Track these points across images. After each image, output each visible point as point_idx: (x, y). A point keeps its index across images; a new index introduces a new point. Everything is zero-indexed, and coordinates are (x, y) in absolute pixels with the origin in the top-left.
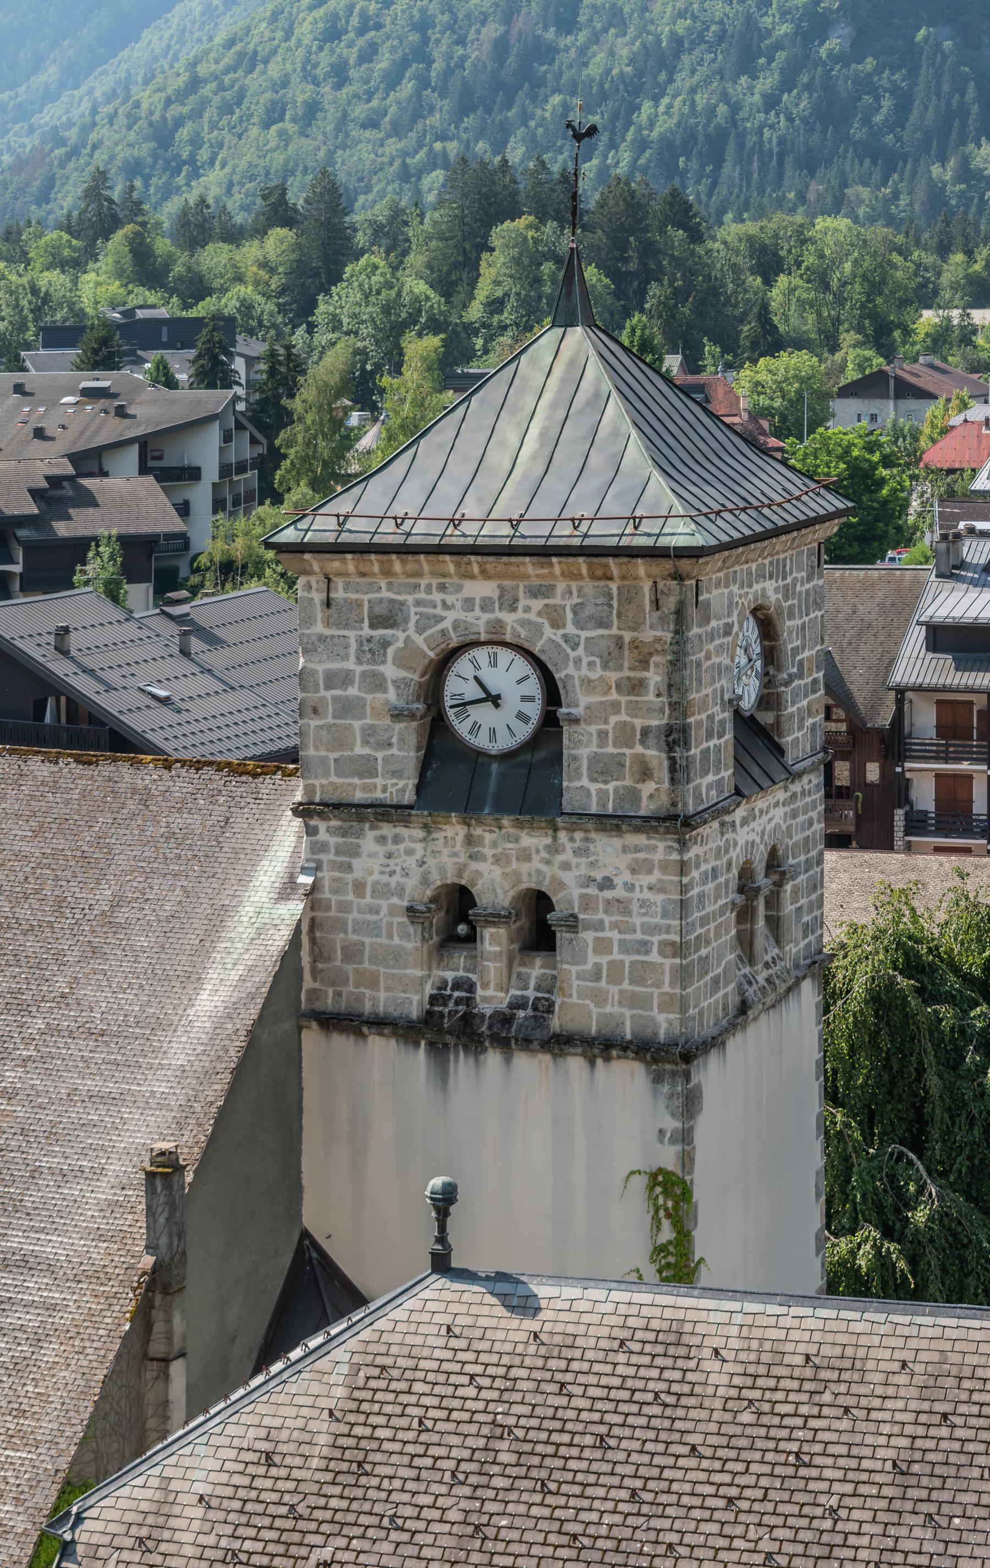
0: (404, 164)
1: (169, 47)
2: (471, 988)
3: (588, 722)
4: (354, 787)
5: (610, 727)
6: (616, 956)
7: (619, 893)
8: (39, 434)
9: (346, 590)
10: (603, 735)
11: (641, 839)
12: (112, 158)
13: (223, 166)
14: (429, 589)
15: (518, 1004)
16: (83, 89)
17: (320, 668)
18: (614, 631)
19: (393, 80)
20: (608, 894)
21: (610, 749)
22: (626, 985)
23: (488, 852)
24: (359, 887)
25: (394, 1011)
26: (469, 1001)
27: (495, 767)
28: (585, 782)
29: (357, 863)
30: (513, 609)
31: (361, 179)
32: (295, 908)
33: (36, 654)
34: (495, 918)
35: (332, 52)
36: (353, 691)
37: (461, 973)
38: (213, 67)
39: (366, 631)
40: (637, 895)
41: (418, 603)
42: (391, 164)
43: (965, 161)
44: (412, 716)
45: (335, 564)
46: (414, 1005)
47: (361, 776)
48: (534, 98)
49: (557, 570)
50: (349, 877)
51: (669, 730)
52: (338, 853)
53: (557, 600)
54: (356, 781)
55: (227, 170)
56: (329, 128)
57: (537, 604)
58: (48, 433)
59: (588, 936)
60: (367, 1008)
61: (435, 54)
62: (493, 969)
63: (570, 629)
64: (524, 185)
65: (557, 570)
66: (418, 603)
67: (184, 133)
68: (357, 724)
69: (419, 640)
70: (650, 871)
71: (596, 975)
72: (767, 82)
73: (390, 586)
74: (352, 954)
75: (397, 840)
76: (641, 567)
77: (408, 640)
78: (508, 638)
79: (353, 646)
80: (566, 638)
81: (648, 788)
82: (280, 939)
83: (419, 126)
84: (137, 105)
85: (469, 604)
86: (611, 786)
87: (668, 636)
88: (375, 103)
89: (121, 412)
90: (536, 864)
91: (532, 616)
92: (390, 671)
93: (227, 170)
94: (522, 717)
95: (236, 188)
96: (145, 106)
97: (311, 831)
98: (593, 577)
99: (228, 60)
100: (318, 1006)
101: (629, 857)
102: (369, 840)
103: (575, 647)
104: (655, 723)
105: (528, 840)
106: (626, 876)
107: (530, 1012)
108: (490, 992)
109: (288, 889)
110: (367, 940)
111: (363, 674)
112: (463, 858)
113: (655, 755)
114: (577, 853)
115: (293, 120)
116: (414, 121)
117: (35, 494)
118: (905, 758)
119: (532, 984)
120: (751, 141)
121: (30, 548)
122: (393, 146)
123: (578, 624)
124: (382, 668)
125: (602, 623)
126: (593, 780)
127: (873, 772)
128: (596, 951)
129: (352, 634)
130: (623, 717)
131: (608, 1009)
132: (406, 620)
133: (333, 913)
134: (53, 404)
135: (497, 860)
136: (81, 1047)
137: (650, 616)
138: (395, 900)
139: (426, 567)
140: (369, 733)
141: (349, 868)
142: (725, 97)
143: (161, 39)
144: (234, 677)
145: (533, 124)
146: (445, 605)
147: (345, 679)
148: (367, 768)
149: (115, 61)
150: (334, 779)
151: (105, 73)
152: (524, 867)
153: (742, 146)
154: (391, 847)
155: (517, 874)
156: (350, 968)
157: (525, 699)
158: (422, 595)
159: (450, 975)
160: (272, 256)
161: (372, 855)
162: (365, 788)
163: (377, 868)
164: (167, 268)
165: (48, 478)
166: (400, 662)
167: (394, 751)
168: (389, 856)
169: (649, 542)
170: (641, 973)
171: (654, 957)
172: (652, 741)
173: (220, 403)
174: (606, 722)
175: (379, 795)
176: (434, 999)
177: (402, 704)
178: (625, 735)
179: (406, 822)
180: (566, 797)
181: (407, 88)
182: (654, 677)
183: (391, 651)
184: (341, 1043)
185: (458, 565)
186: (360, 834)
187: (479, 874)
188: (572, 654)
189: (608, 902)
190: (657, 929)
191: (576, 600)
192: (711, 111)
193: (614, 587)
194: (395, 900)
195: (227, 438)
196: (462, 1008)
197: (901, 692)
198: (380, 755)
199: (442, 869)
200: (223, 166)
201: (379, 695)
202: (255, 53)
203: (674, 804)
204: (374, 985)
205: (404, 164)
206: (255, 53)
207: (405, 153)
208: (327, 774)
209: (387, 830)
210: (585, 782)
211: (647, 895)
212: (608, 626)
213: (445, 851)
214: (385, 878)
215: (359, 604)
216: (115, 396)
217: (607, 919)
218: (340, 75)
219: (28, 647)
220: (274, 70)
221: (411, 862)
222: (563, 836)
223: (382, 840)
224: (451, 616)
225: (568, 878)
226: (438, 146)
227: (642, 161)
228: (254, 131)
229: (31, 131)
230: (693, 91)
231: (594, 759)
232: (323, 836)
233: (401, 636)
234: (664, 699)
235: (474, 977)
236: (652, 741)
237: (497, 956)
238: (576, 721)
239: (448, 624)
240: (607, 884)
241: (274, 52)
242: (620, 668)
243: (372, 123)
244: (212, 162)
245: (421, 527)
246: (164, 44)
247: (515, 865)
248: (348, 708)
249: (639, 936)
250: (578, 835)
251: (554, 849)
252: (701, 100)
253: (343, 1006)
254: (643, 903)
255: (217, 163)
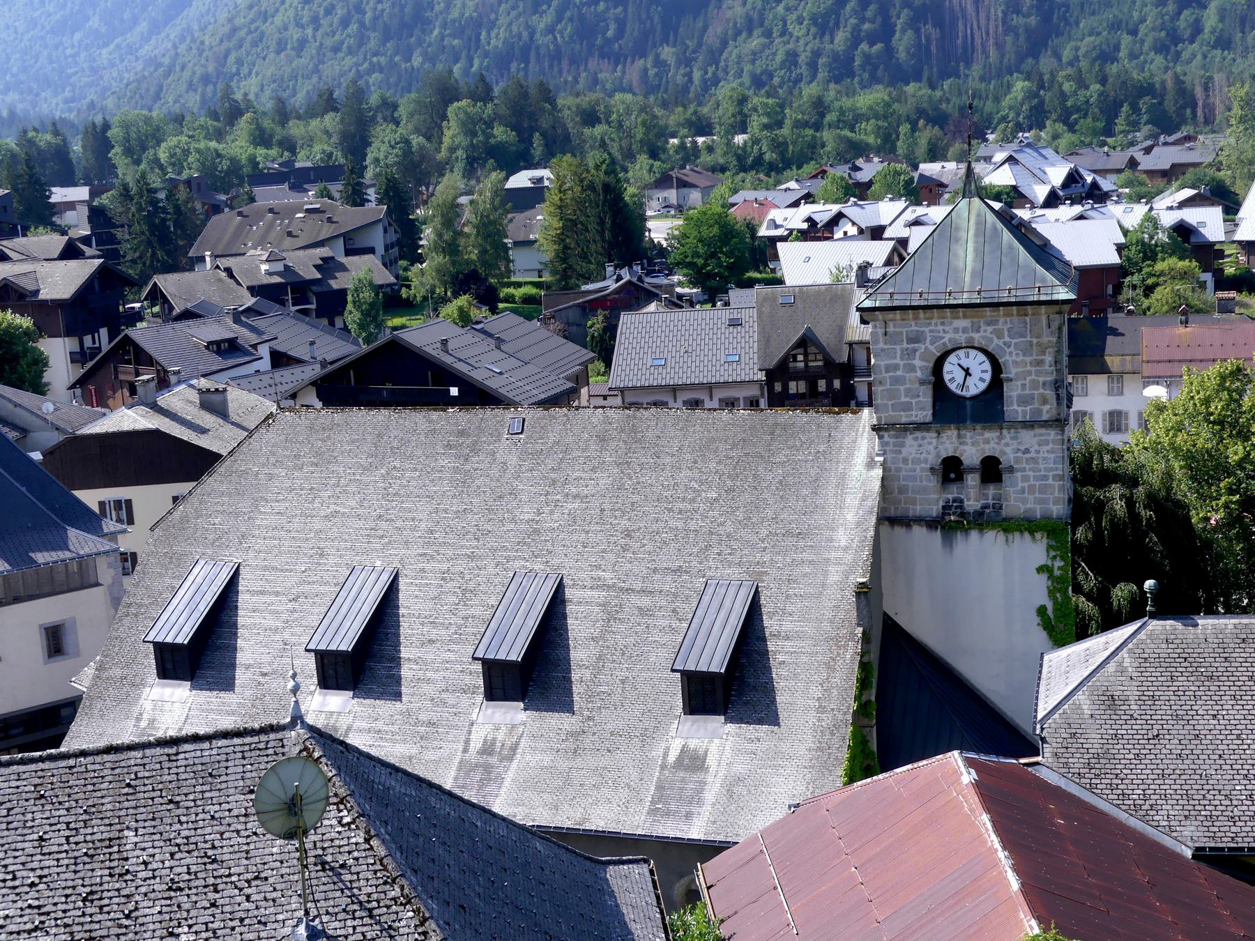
0: (358, 71)
1: (209, 9)
2: (961, 501)
3: (1016, 380)
4: (901, 416)
5: (1027, 382)
6: (1032, 482)
7: (1033, 455)
8: (290, 234)
9: (894, 327)
10: (1024, 386)
11: (1043, 431)
12: (194, 73)
13: (257, 74)
14: (936, 325)
15: (985, 507)
16: (163, 35)
17: (883, 363)
18: (1028, 339)
19: (345, 23)
20: (1027, 456)
21: (1027, 392)
22: (1037, 495)
23: (969, 441)
24: (905, 461)
25: (924, 514)
26: (961, 507)
27: (968, 402)
28: (1015, 407)
29: (904, 450)
30: (978, 331)
31: (335, 80)
32: (878, 472)
33: (434, 353)
34: (972, 470)
35: (310, 10)
36: (899, 373)
37: (956, 495)
38: (243, 20)
39: (905, 345)
40: (1041, 455)
41: (931, 331)
42: (350, 71)
43: (657, 56)
44: (930, 383)
45: (890, 315)
46: (935, 510)
47: (904, 411)
48: (423, 31)
49: (1001, 313)
50: (900, 456)
51: (1056, 382)
52: (894, 446)
53: (1000, 326)
54: (902, 413)
55: (260, 77)
56: (314, 52)
57: (990, 329)
58: (294, 234)
59: (1019, 475)
60: (911, 514)
61: (367, 9)
62: (973, 492)
63: (1007, 339)
64: (462, 84)
65: (1001, 313)
66: (931, 331)
67: (232, 58)
68: (902, 388)
69: (932, 348)
70: (1048, 444)
71: (1023, 491)
72: (548, 18)
73: (916, 324)
74: (902, 490)
75: (923, 438)
76: (1043, 309)
77: (926, 348)
78: (976, 345)
79: (899, 353)
80: (1005, 343)
81: (1046, 408)
82: (876, 485)
83: (363, 49)
84: (202, 43)
85: (956, 330)
86: (1028, 408)
87: (1055, 340)
88: (337, 37)
89: (330, 220)
90: (992, 445)
91: (988, 334)
92: (918, 362)
93: (260, 77)
94: (982, 380)
95: (266, 88)
96: (207, 43)
97: (880, 437)
98: (1018, 315)
99: (251, 15)
100: (887, 514)
101: (1037, 439)
102: (909, 440)
103: (1009, 347)
104: (1049, 379)
105: (988, 435)
106: (1036, 447)
107: (991, 509)
108: (971, 503)
109: (871, 464)
110: (910, 484)
111: (904, 365)
112: (957, 444)
113: (1050, 393)
114: (1012, 438)
115: (293, 49)
116: (359, 47)
117: (317, 267)
118: (853, 377)
119: (990, 497)
120: (542, 51)
121: (317, 295)
122: (349, 61)
123: (1011, 336)
124: (914, 362)
125: (1022, 336)
126: (1019, 406)
127: (837, 384)
128: (1022, 481)
129: (898, 347)
130: (1033, 377)
131: (1029, 506)
132: (925, 340)
133: (893, 473)
134: (292, 219)
135: (973, 444)
136: (790, 541)
137: (1046, 331)
138: (923, 465)
139: (936, 315)
140: (908, 391)
141: (900, 452)
142: (527, 26)
143: (204, 5)
144: (525, 356)
145: (425, 45)
146: (944, 331)
147: (896, 367)
148: (907, 407)
149: (179, 18)
150: (891, 413)
151: (174, 25)
152: (987, 446)
153: (538, 54)
154: (920, 442)
155: (983, 450)
156: (902, 497)
157: (983, 372)
158: (933, 328)
159: (950, 497)
160: (329, 128)
161: (911, 446)
162: (906, 416)
163: (914, 452)
164: (271, 136)
165: (322, 259)
166: (922, 358)
167: (921, 399)
168: (920, 446)
169: (1049, 298)
170: (1044, 489)
171: (1050, 481)
172: (1047, 387)
173: (381, 213)
174: (1025, 379)
175: (914, 419)
176: (944, 507)
177: (924, 377)
178: (1034, 385)
179: (928, 430)
180: (1006, 414)
181: (354, 27)
182: (1048, 358)
183: (917, 354)
184: (899, 531)
185: (952, 313)
186: (905, 437)
187: (965, 451)
188: (1008, 350)
189: (1027, 459)
190: (1051, 469)
191: (1009, 326)
192: (519, 36)
193: (1028, 319)
194: (923, 465)
195: (385, 231)
196: (959, 510)
197: (851, 344)
198: (914, 401)
199: (946, 450)
200: (257, 74)
201: (913, 374)
202: (266, 12)
203: (1059, 414)
204: (914, 503)
205: (358, 71)
206: (266, 12)
207: (357, 65)
208: (887, 411)
209: (918, 434)
210: (1015, 407)
211: (1046, 455)
212: (1025, 337)
213: (948, 442)
214: (918, 456)
215: (901, 333)
216: (324, 212)
217: (1027, 467)
218: (315, 21)
219: (428, 350)
220: (278, 20)
221: (931, 448)
222: (1005, 432)
223: (916, 439)
224: (947, 337)
225: (1008, 450)
226: (375, 59)
227: (485, 64)
228: (272, 56)
229: (137, 59)
230: (510, 24)
231: (1019, 396)
232: (886, 439)
233: (923, 346)
234: (1053, 368)
235: (962, 497)
236: (1047, 387)
237: (974, 487)
238: (1010, 380)
239: (946, 340)
240: (1027, 451)
241: (277, 10)
242: (1032, 355)
243: (336, 49)
244: (250, 73)
245: (931, 296)
246: (206, 7)
247: (982, 446)
248: (897, 381)
249: (1043, 473)
250: (1012, 431)
251: (1001, 437)
252: (515, 28)
253: (899, 513)
254: (1044, 459)
255: (253, 74)
